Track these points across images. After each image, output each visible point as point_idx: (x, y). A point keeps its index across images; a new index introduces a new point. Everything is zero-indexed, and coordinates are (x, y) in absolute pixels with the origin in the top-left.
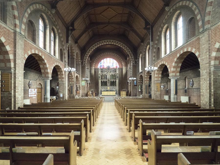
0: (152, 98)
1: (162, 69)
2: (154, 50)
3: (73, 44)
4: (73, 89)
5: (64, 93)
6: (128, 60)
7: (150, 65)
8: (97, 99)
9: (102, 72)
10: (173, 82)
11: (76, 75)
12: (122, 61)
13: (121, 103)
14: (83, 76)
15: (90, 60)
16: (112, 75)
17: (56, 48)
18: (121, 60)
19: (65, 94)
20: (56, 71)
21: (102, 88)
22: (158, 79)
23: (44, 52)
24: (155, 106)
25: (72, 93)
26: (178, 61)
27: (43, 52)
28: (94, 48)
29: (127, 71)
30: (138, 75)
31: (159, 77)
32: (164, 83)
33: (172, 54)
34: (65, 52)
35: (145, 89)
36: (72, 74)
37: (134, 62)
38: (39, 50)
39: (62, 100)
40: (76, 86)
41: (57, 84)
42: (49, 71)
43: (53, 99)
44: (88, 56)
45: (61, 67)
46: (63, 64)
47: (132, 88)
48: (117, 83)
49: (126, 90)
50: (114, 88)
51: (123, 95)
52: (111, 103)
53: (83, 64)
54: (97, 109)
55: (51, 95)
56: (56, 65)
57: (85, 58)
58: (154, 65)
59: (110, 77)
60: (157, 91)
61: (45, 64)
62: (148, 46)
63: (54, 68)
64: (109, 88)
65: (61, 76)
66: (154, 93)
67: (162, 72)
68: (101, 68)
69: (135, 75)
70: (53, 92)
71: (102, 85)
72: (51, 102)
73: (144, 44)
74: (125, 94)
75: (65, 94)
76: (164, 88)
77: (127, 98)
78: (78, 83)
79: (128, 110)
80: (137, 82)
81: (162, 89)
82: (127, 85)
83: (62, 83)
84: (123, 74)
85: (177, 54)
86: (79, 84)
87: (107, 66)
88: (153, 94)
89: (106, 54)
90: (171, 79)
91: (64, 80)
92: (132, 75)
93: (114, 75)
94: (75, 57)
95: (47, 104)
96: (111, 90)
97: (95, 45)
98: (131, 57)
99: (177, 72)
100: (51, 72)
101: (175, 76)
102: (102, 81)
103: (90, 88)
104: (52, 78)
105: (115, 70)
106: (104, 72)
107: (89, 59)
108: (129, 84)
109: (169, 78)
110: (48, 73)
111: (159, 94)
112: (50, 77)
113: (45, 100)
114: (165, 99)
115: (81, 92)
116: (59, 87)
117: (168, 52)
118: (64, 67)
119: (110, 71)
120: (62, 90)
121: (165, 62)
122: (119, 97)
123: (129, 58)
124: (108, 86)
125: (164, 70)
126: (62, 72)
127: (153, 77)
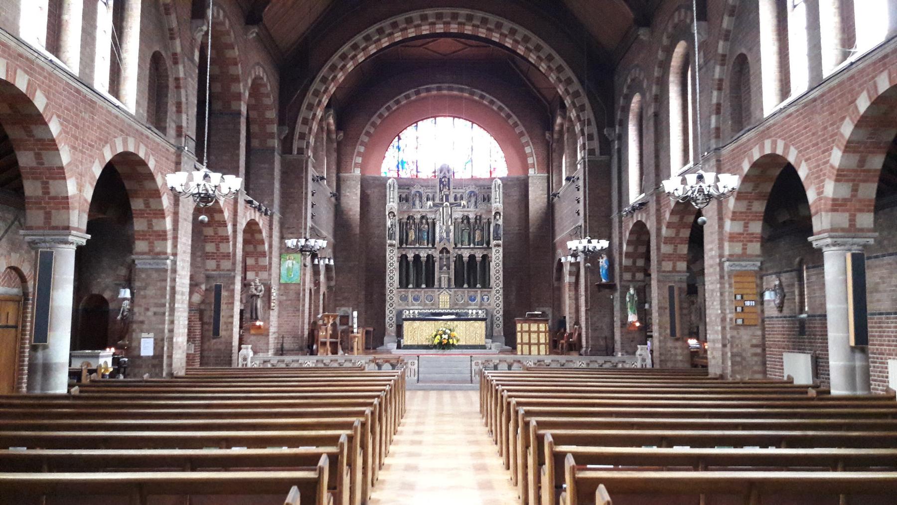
0: (714, 369)
1: (768, 188)
2: (718, 69)
3: (231, 26)
4: (223, 307)
5: (163, 331)
6: (561, 132)
7: (691, 164)
8: (371, 368)
9: (407, 200)
10: (835, 268)
11: (246, 215)
12: (525, 139)
13: (519, 404)
14: (289, 227)
15: (333, 127)
16: (468, 218)
17: (124, 46)
18: (521, 128)
19: (169, 337)
20: (121, 189)
21: (404, 299)
22: (744, 249)
23: (48, 68)
24: (735, 427)
25: (216, 333)
26: (863, 134)
27: (43, 69)
28: (361, 58)
29: (555, 195)
30: (621, 222)
31: (751, 238)
32: (778, 274)
33: (822, 95)
34: (182, 75)
35: (668, 311)
36: (221, 212)
37: (596, 144)
38: (20, 56)
39: (146, 376)
40: (246, 285)
41: (123, 272)
42: (71, 187)
43: (95, 371)
44: (325, 101)
45: (152, 164)
46: (167, 146)
47: (582, 300)
48: (492, 272)
49: (549, 311)
50: (478, 299)
51: (530, 344)
52: (459, 394)
53: (295, 152)
54: (364, 447)
55: (73, 347)
56: (120, 150)
57: (304, 112)
58: (718, 161)
59: (452, 234)
60: (740, 322)
61: (52, 145)
62: (680, 49)
63: (109, 170)
64: (444, 299)
65: (150, 225)
66: (724, 338)
67: (765, 203)
68: (398, 178)
69: (599, 220)
70: (96, 325)
71: (404, 283)
72: (75, 390)
73: (652, 32)
74: (542, 341)
75: (171, 339)
76: (780, 307)
77: (553, 365)
78: (258, 269)
79: (563, 455)
80: (617, 267)
81: (771, 310)
82: (556, 284)
83: (157, 270)
84: (530, 221)
85: (859, 94)
86: (264, 275)
87: (438, 167)
88: (714, 341)
89: (434, 93)
90: (824, 249)
91: (169, 250)
92: (581, 222)
93: (478, 218)
94: (244, 109)
95: (46, 407)
96: (457, 314)
97: (367, 38)
98: (575, 118)
99: (858, 206)
100: (89, 194)
101: (843, 230)
102: (403, 259)
103: (335, 297)
104: (88, 232)
105: (481, 191)
106: (417, 202)
107: (331, 121)
108: (567, 279)
109: (811, 243)
110: (64, 202)
111: (754, 342)
112: (77, 229)
113: (39, 377)
114: (790, 380)
115: (273, 322)
116: (132, 293)
117: (800, 83)
118: (173, 166)
119: (455, 199)
120: (150, 313)
121: (786, 147)
122: (510, 357)
123: (564, 117)
124: (440, 287)
125: (779, 197)
126: (157, 194)
127: (716, 237)
